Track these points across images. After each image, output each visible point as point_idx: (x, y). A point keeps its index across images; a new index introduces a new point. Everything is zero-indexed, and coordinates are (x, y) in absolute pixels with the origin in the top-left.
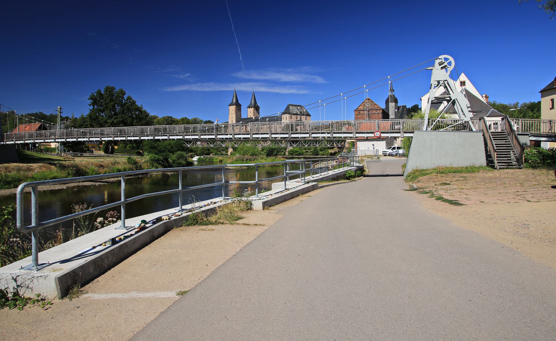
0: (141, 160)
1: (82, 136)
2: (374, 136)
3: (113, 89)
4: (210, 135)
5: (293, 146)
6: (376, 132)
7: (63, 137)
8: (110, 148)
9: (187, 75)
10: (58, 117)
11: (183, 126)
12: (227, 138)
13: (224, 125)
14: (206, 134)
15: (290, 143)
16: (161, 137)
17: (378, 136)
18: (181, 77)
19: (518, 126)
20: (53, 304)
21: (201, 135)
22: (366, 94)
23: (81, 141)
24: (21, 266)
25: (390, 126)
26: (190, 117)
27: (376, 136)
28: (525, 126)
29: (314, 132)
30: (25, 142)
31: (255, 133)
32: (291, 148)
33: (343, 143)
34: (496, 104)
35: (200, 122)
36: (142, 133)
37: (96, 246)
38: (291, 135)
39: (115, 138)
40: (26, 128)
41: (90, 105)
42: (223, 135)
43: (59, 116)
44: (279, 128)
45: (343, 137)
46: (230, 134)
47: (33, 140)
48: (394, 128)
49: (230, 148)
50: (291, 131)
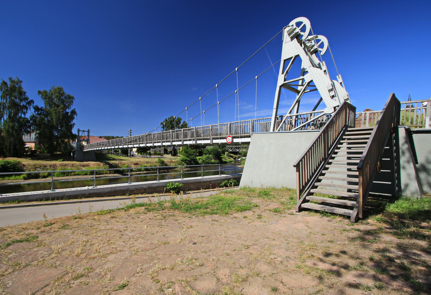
1: (165, 140)
4: (246, 137)
9: (250, 106)
16: (189, 142)
18: (246, 108)
19: (418, 127)
21: (213, 139)
22: (203, 115)
23: (201, 144)
24: (306, 69)
25: (229, 130)
26: (115, 136)
28: (334, 131)
29: (206, 137)
30: (198, 143)
35: (119, 137)
37: (85, 130)
39: (198, 141)
41: (162, 128)
42: (239, 138)
47: (194, 140)
48: (245, 132)
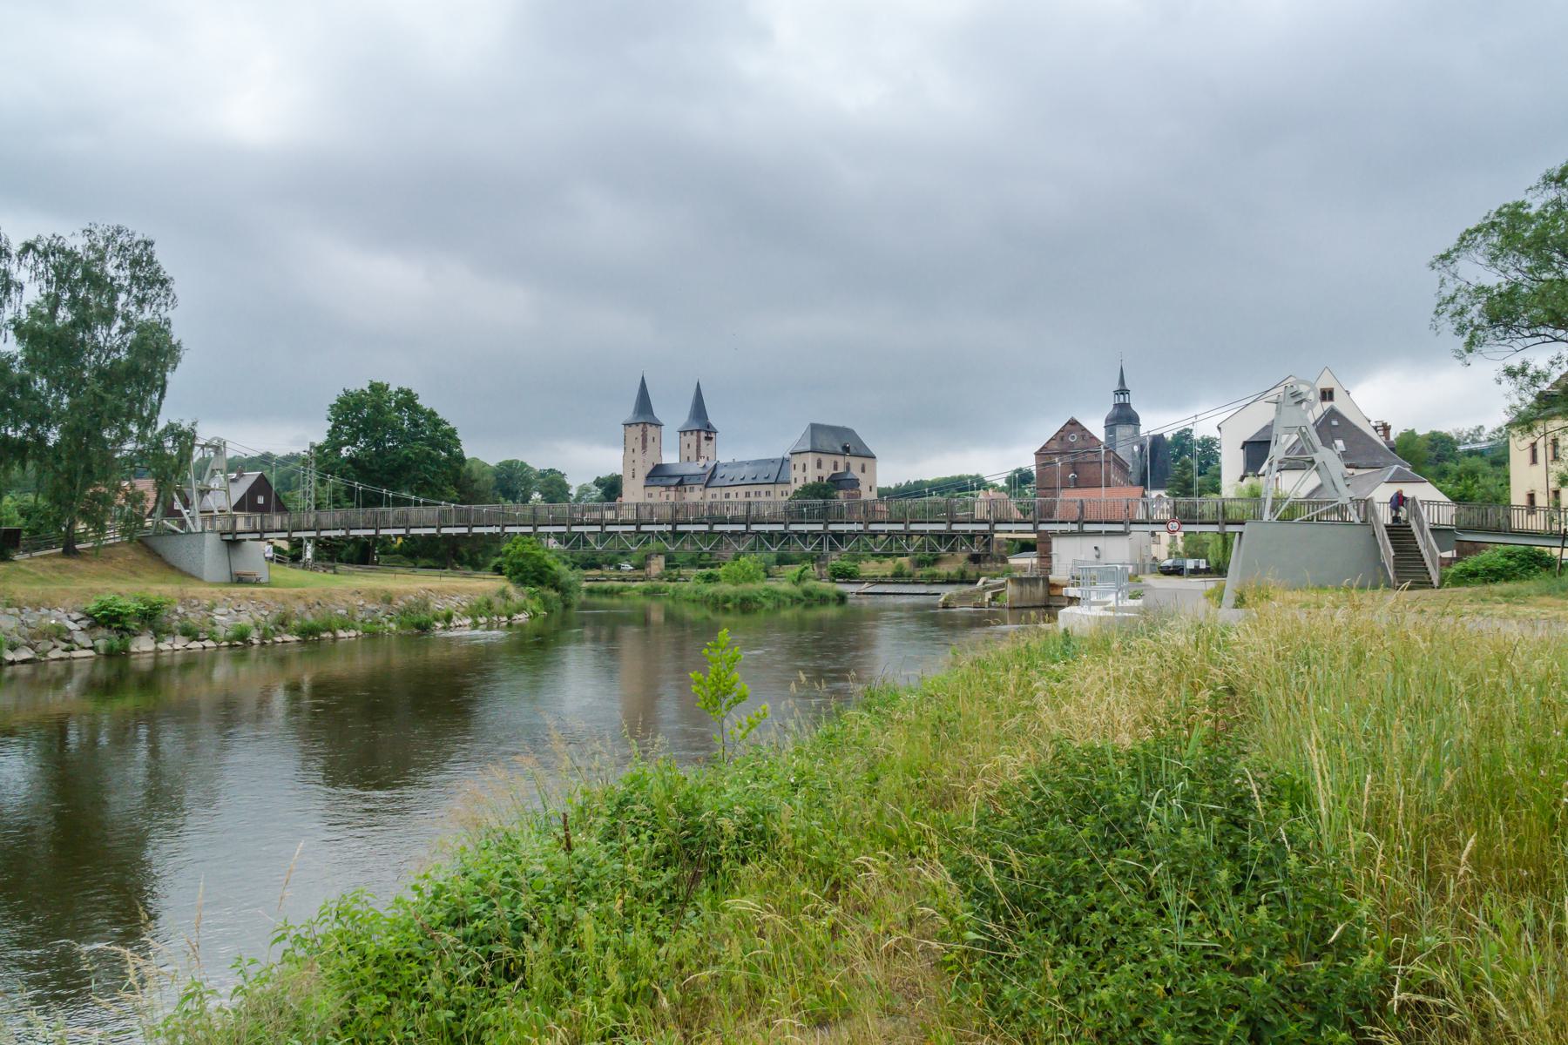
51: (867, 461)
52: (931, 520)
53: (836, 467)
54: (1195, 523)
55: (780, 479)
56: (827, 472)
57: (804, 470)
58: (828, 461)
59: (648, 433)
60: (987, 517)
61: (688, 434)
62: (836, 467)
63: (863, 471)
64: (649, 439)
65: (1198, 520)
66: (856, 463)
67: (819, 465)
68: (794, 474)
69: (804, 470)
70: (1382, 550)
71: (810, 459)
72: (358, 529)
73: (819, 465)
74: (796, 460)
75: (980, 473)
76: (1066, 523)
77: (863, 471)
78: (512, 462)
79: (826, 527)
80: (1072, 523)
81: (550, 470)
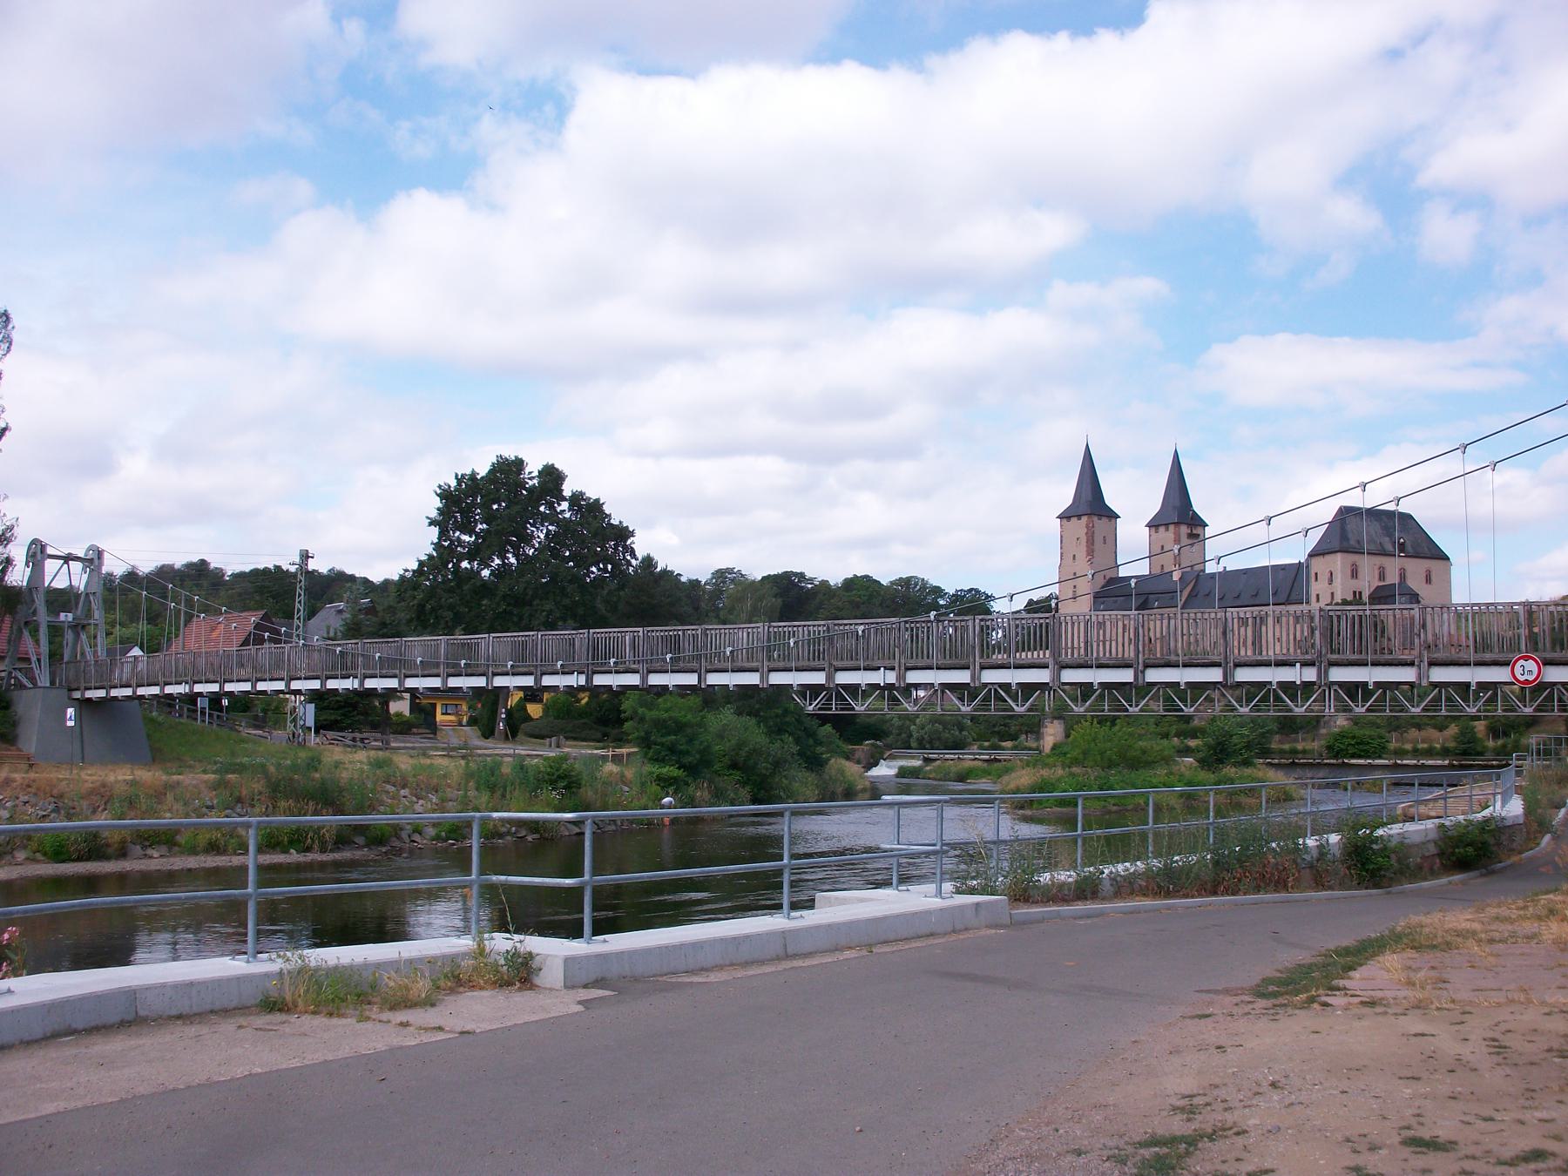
0: (144, 808)
2: (1509, 679)
3: (519, 464)
5: (1351, 710)
6: (1522, 662)
7: (373, 672)
8: (503, 716)
10: (298, 589)
11: (699, 632)
12: (876, 686)
13: (862, 627)
14: (788, 665)
15: (1338, 698)
17: (1531, 678)
20: (1450, 1069)
27: (1522, 679)
31: (713, 667)
32: (1341, 722)
33: (655, 757)
34: (479, 477)
36: (597, 661)
38: (1143, 672)
40: (213, 629)
43: (301, 588)
44: (1277, 639)
45: (1274, 683)
46: (885, 668)
49: (1047, 723)
50: (982, 657)
51: (1434, 565)
52: (1379, 657)
53: (1382, 576)
54: (1467, 664)
55: (1293, 597)
56: (1367, 583)
57: (1331, 581)
58: (1368, 565)
59: (1096, 530)
60: (1130, 653)
61: (1162, 529)
62: (1382, 576)
63: (1428, 580)
64: (1098, 539)
65: (267, 676)
66: (1416, 570)
67: (1355, 574)
68: (1317, 588)
69: (1331, 581)
70: (585, 743)
71: (1338, 562)
72: (1175, 665)
73: (1355, 574)
74: (1319, 565)
75: (387, 577)
76: (1291, 664)
77: (1428, 580)
78: (909, 579)
79: (830, 678)
80: (1305, 664)
81: (971, 590)
